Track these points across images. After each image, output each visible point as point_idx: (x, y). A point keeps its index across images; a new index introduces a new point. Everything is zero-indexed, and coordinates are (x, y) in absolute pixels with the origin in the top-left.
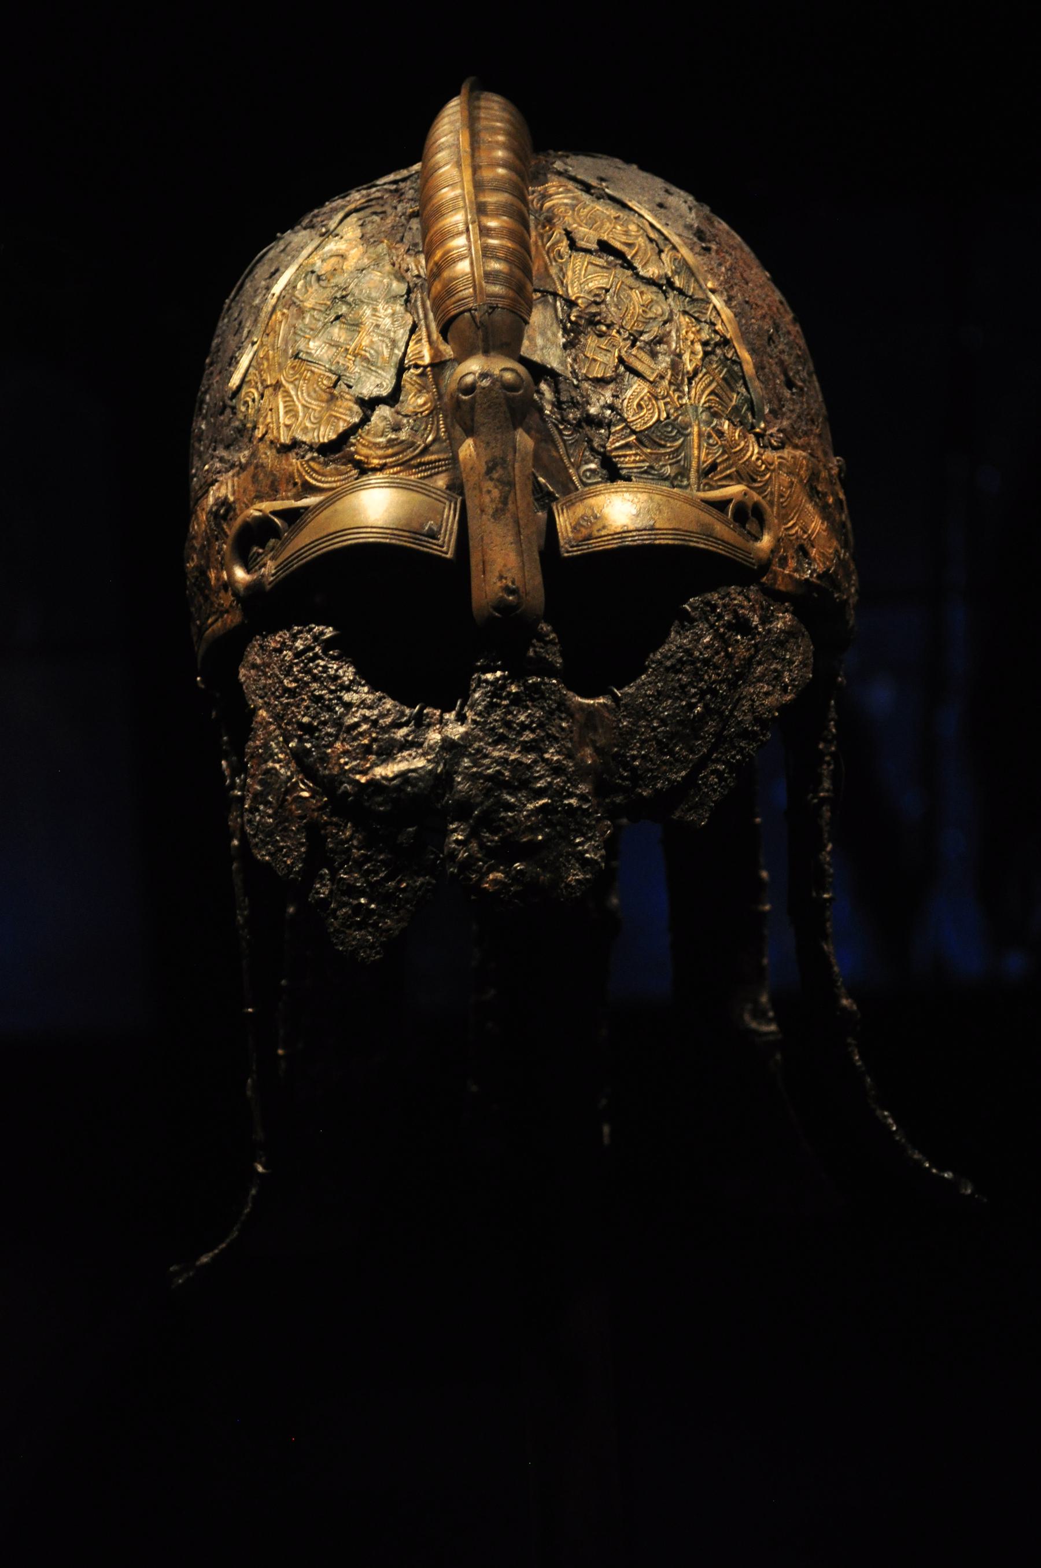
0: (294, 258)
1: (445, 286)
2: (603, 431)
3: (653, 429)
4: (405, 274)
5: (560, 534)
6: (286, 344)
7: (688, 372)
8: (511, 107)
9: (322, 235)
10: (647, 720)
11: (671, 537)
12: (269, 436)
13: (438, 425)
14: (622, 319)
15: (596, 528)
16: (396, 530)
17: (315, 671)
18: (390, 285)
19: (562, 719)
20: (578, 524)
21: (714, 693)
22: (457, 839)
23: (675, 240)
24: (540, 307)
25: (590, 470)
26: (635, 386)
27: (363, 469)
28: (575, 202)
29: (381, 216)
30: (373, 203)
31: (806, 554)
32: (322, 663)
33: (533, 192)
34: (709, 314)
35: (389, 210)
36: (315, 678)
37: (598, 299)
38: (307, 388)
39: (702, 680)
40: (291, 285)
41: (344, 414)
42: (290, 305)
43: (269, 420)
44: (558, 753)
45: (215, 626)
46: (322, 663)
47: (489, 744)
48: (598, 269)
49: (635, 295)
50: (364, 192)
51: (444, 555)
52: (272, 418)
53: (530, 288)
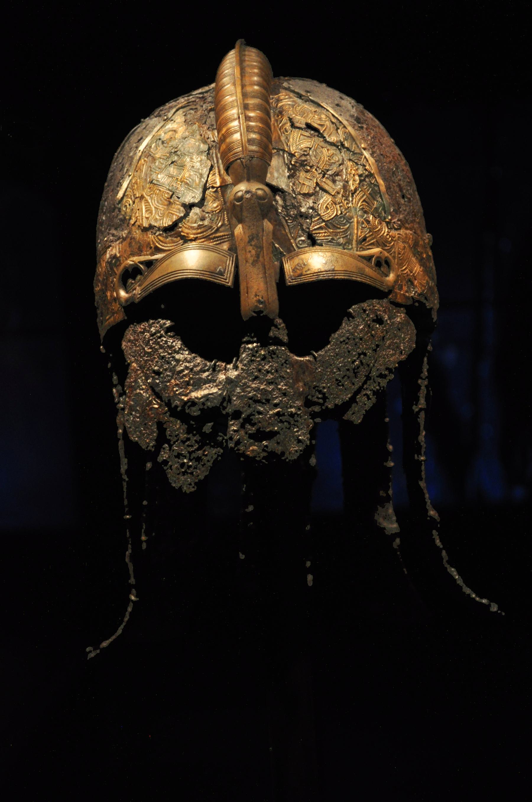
0: (150, 132)
1: (227, 147)
2: (308, 220)
3: (334, 219)
4: (207, 140)
5: (286, 273)
6: (146, 176)
7: (352, 190)
8: (261, 53)
9: (165, 120)
10: (330, 368)
11: (343, 275)
12: (138, 223)
13: (224, 217)
14: (318, 163)
15: (304, 270)
16: (203, 271)
17: (161, 343)
18: (199, 146)
19: (287, 368)
20: (296, 268)
21: (365, 354)
22: (234, 429)
23: (345, 123)
24: (276, 157)
25: (302, 240)
26: (325, 198)
27: (186, 240)
28: (294, 103)
29: (195, 110)
30: (191, 104)
31: (412, 283)
32: (165, 339)
33: (273, 98)
34: (363, 161)
35: (199, 108)
36: (161, 347)
37: (306, 153)
38: (157, 198)
39: (359, 348)
40: (149, 146)
41: (176, 212)
42: (148, 156)
43: (137, 215)
44: (286, 385)
45: (110, 320)
46: (165, 339)
47: (250, 381)
48: (306, 138)
49: (325, 151)
50: (186, 98)
51: (227, 284)
52: (139, 214)
53: (271, 147)
